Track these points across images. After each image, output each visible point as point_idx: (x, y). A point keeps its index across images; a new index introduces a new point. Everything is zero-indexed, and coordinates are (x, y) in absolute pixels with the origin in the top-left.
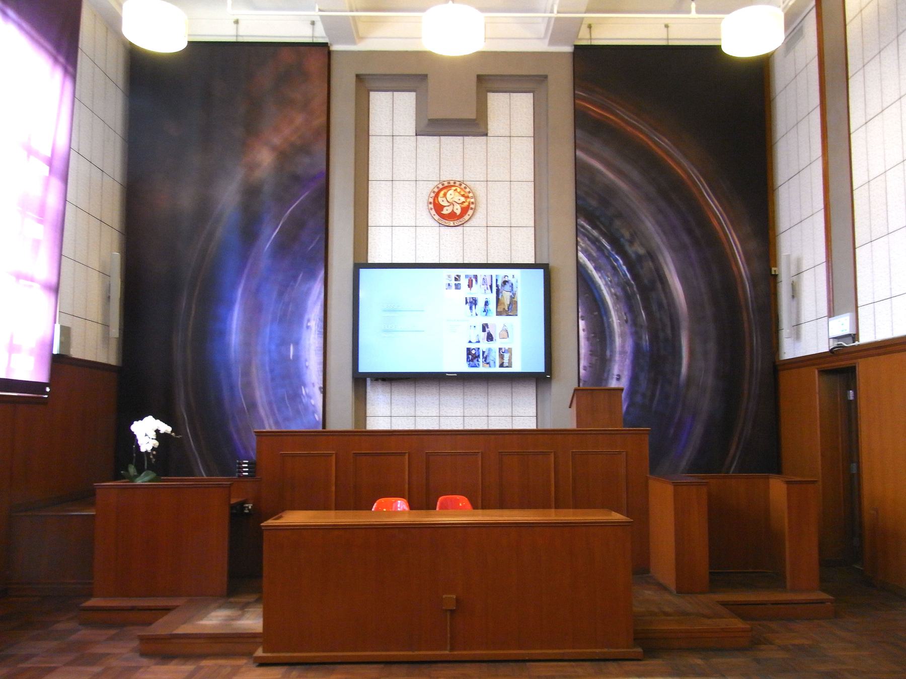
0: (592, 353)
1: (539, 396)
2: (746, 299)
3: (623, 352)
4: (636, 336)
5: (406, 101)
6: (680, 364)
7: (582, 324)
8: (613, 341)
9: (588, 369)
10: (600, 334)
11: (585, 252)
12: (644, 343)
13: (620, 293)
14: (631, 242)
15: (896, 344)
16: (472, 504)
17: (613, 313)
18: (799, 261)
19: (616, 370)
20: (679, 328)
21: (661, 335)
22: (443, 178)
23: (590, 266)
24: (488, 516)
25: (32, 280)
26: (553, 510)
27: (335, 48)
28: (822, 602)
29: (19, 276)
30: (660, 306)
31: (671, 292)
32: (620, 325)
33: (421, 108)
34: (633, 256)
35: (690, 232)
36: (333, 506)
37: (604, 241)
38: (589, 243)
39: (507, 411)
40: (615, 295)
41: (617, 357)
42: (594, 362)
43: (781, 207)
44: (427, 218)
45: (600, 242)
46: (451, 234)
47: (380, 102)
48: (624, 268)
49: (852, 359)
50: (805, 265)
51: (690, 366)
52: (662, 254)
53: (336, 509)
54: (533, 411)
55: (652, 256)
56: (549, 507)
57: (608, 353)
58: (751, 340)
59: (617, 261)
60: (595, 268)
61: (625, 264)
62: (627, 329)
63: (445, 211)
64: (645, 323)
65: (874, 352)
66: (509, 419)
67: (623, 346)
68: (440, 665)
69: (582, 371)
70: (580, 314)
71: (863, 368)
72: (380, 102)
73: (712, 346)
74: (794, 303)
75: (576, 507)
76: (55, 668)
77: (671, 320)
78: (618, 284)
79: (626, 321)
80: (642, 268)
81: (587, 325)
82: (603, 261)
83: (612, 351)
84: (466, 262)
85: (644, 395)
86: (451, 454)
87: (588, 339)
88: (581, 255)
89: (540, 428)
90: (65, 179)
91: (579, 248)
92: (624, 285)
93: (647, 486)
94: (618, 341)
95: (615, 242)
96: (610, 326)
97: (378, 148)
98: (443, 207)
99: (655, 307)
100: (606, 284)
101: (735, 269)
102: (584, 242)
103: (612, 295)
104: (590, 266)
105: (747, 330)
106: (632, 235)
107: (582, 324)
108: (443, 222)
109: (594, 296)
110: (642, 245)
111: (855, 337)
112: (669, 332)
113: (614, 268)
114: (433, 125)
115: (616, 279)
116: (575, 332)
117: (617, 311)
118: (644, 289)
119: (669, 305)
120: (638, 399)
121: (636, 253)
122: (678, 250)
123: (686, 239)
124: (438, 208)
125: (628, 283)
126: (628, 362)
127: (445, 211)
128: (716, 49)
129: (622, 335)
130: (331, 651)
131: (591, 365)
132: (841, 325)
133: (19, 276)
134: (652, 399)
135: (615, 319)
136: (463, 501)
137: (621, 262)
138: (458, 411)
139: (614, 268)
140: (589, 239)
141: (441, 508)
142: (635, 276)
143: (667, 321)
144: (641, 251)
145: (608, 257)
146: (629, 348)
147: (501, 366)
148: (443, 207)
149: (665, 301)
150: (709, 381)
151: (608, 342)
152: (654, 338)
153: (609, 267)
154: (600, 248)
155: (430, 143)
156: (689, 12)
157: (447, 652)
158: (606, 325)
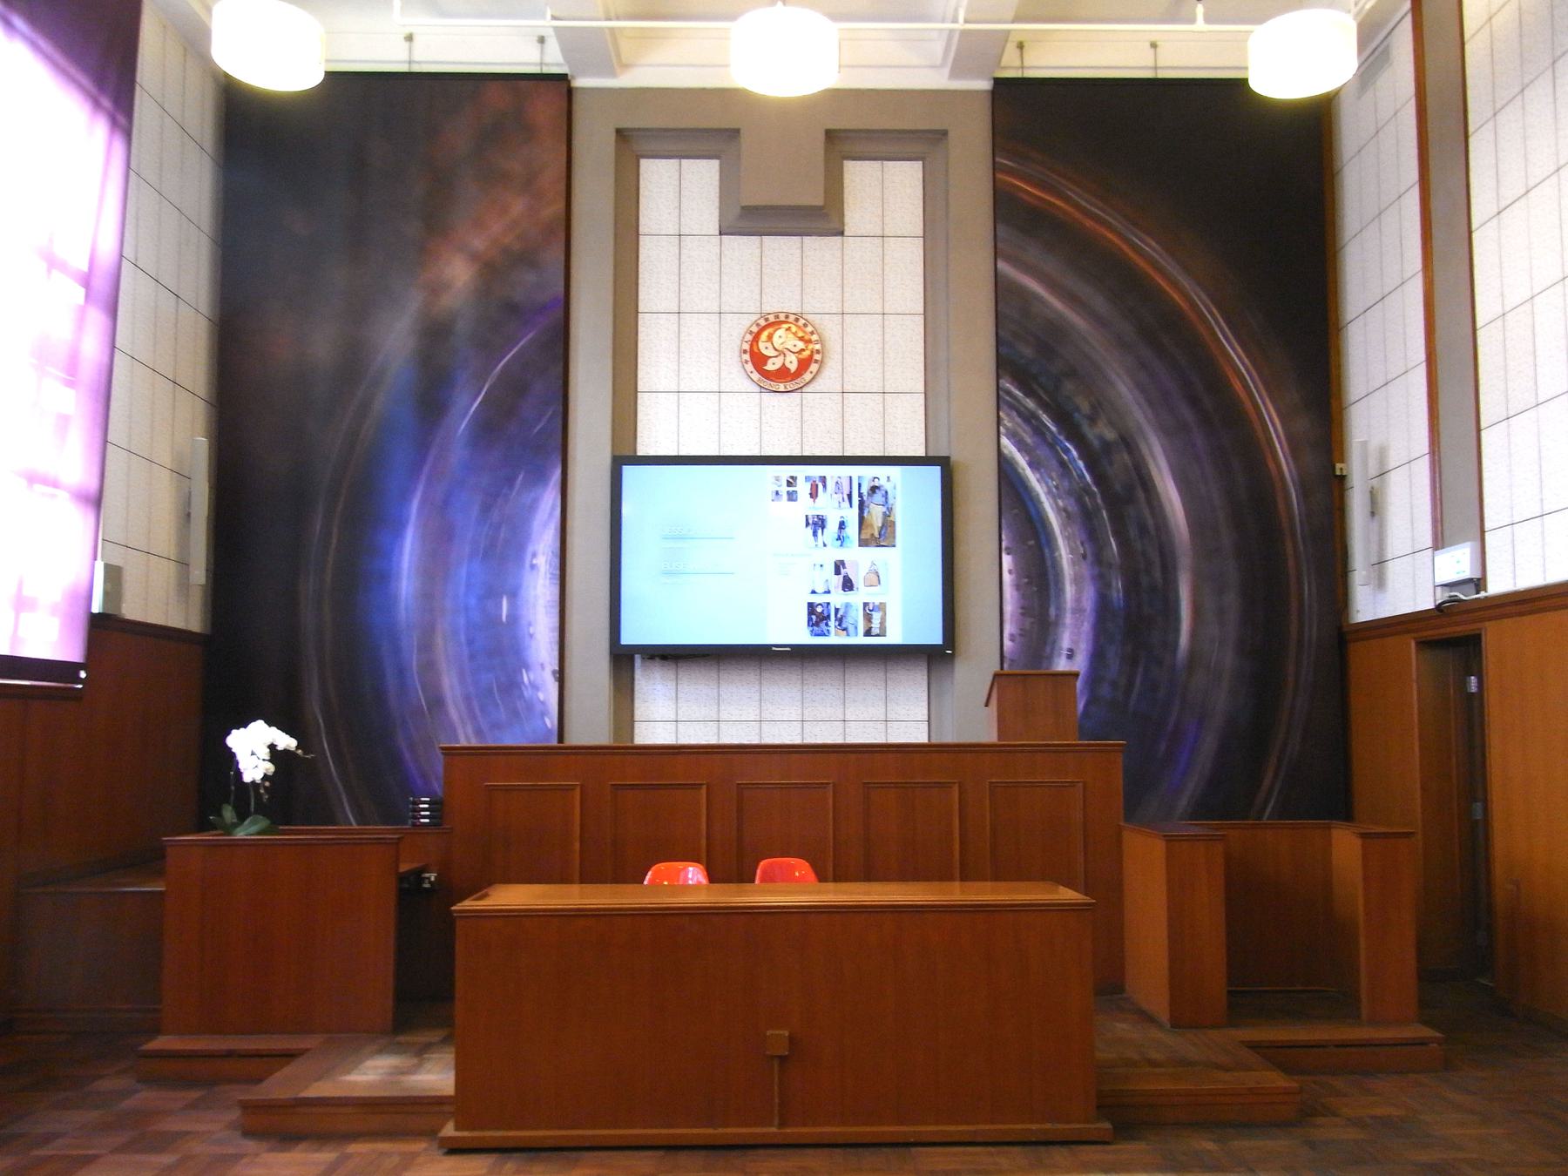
0: (1025, 611)
1: (933, 686)
2: (1291, 518)
3: (1078, 610)
4: (1102, 581)
5: (703, 176)
6: (1177, 630)
7: (1007, 560)
8: (1060, 591)
9: (1018, 639)
10: (1039, 579)
11: (1013, 436)
12: (1115, 594)
13: (1073, 508)
14: (1092, 420)
15: (1551, 596)
16: (817, 874)
17: (1061, 542)
18: (1383, 453)
19: (1065, 642)
20: (1175, 568)
21: (1144, 580)
22: (767, 309)
23: (1021, 461)
24: (845, 893)
25: (55, 484)
26: (957, 884)
27: (580, 82)
28: (1423, 1042)
29: (33, 479)
30: (1143, 529)
31: (1161, 506)
32: (1073, 563)
33: (728, 186)
34: (1096, 443)
35: (1194, 401)
36: (577, 876)
37: (1045, 418)
38: (1019, 420)
39: (877, 712)
40: (1065, 510)
41: (1068, 619)
42: (1027, 626)
43: (1351, 359)
44: (738, 377)
45: (1038, 418)
46: (781, 406)
47: (657, 176)
48: (1081, 464)
49: (1474, 622)
50: (1393, 460)
51: (1194, 634)
52: (1146, 440)
53: (582, 881)
54: (922, 712)
55: (1128, 443)
56: (951, 878)
57: (1052, 611)
58: (1300, 588)
59: (1067, 451)
60: (1030, 464)
61: (1081, 457)
62: (1086, 570)
63: (771, 366)
64: (1117, 560)
65: (1513, 609)
66: (881, 726)
67: (1078, 600)
68: (761, 1152)
69: (1007, 643)
70: (1004, 544)
71: (1494, 637)
72: (657, 176)
73: (1232, 599)
74: (1375, 526)
75: (996, 877)
76: (95, 1158)
77: (1162, 554)
78: (1070, 493)
79: (1084, 557)
80: (1111, 464)
81: (1016, 562)
82: (1043, 452)
83: (1060, 609)
84: (806, 454)
85: (1114, 684)
86: (781, 787)
87: (1018, 587)
88: (1005, 441)
89: (934, 741)
90: (112, 310)
91: (1002, 429)
92: (1079, 494)
93: (1119, 842)
94: (1069, 591)
95: (1064, 419)
96: (1056, 564)
97: (654, 256)
98: (766, 358)
99: (1133, 532)
100: (1049, 492)
101: (1272, 465)
102: (1012, 419)
103: (1060, 511)
104: (1021, 461)
105: (1292, 572)
106: (1093, 407)
107: (1007, 560)
108: (767, 384)
109: (1027, 513)
110: (1111, 424)
111: (1479, 583)
112: (1158, 574)
113: (1062, 464)
114: (749, 217)
115: (1066, 484)
116: (995, 575)
117: (1067, 538)
118: (1115, 501)
119: (1158, 529)
120: (1105, 690)
121: (1101, 439)
122: (1173, 432)
123: (1187, 414)
124: (758, 360)
125: (1086, 490)
126: (1086, 627)
127: (771, 366)
128: (1240, 85)
129: (1077, 580)
130: (573, 1128)
131: (1023, 633)
132: (1456, 564)
133: (33, 479)
134: (1128, 692)
135: (1065, 553)
136: (801, 867)
137: (1075, 453)
138: (793, 712)
139: (1062, 464)
140: (1020, 414)
141: (763, 880)
142: (1100, 479)
143: (1154, 556)
144: (1110, 435)
145: (1052, 445)
146: (1088, 603)
147: (868, 633)
148: (766, 358)
149: (1150, 522)
150: (1228, 659)
151: (1052, 592)
152: (1132, 585)
153: (1054, 462)
154: (1039, 430)
155: (744, 248)
156: (1192, 20)
157: (774, 1130)
158: (1049, 563)
